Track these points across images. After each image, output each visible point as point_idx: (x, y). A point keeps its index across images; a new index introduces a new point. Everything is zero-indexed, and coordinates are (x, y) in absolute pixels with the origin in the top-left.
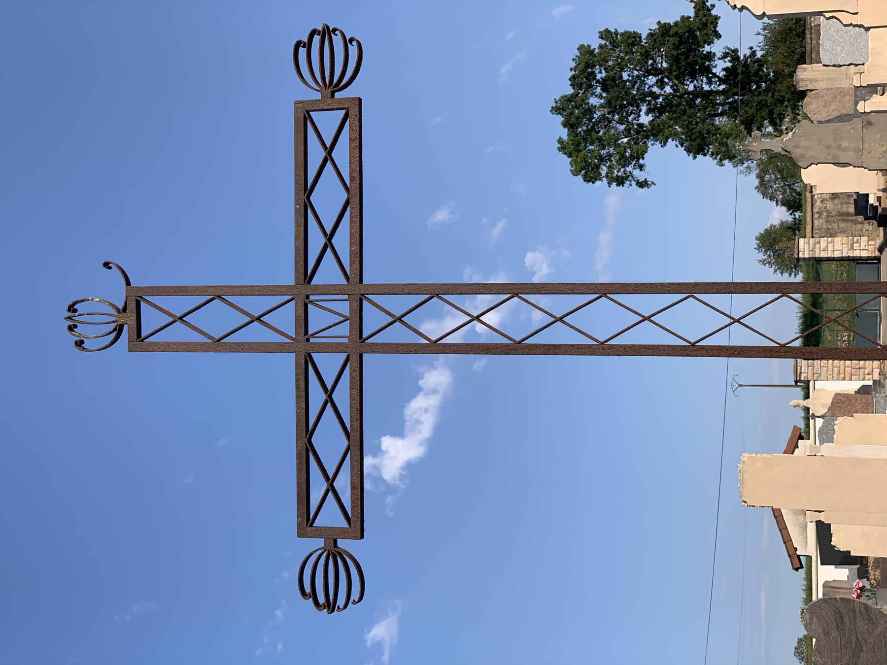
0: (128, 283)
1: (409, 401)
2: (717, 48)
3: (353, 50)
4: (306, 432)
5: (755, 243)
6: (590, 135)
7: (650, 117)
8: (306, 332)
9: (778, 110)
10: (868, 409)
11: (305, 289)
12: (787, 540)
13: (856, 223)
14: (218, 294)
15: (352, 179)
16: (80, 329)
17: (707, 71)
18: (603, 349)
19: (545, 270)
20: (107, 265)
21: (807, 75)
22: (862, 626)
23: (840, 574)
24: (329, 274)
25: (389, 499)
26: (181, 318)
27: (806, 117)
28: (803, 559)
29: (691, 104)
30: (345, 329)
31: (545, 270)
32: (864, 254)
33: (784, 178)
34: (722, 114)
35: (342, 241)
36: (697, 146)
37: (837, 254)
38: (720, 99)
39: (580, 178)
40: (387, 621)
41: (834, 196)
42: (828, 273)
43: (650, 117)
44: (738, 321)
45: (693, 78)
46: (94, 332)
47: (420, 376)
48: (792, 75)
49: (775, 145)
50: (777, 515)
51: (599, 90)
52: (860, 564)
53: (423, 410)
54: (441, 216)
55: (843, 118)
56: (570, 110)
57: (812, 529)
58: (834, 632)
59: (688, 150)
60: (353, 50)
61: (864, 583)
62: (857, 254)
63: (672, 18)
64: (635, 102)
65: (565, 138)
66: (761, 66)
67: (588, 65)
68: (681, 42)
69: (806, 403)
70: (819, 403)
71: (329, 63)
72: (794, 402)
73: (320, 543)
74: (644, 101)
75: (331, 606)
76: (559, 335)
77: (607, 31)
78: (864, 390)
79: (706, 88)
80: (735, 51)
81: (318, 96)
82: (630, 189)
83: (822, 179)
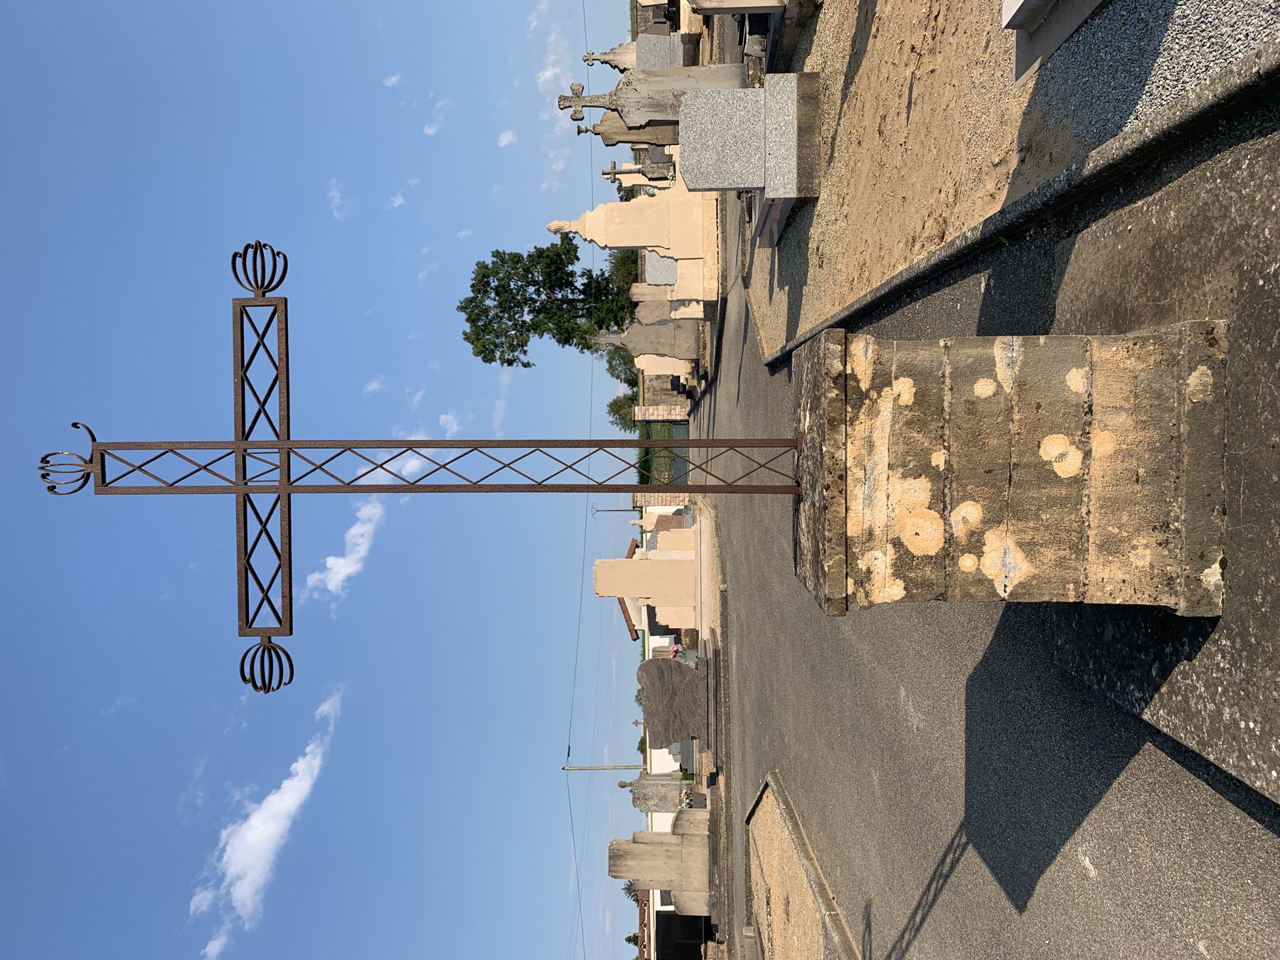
0: (94, 440)
1: (348, 528)
2: (577, 268)
3: (280, 261)
4: (245, 554)
5: (606, 409)
6: (486, 328)
7: (531, 317)
8: (245, 477)
9: (620, 315)
10: (680, 525)
11: (243, 445)
12: (628, 620)
13: (672, 396)
14: (171, 448)
15: (280, 359)
16: (52, 477)
17: (570, 284)
18: (475, 487)
19: (455, 428)
20: (75, 425)
21: (638, 291)
22: (676, 678)
23: (664, 642)
24: (262, 432)
25: (333, 605)
26: (139, 468)
27: (639, 322)
28: (640, 633)
29: (560, 308)
30: (276, 475)
31: (455, 428)
32: (678, 418)
33: (625, 364)
34: (582, 316)
35: (273, 407)
36: (565, 338)
37: (660, 418)
38: (580, 305)
39: (479, 358)
40: (332, 699)
41: (658, 377)
42: (657, 432)
43: (531, 317)
44: (381, 466)
45: (561, 289)
46: (65, 479)
47: (359, 509)
48: (628, 290)
49: (616, 339)
50: (622, 602)
51: (493, 295)
52: (676, 633)
53: (360, 535)
54: (373, 386)
55: (663, 322)
56: (472, 309)
57: (644, 609)
58: (658, 683)
59: (559, 341)
60: (280, 261)
61: (680, 647)
62: (673, 418)
63: (545, 245)
64: (520, 305)
65: (468, 330)
66: (608, 283)
67: (484, 276)
68: (552, 262)
69: (640, 522)
70: (649, 522)
71: (261, 270)
72: (632, 522)
73: (257, 640)
74: (525, 303)
75: (267, 688)
76: (507, 477)
77: (497, 251)
78: (678, 513)
79: (570, 296)
80: (590, 271)
81: (252, 295)
82: (517, 369)
83: (647, 364)
